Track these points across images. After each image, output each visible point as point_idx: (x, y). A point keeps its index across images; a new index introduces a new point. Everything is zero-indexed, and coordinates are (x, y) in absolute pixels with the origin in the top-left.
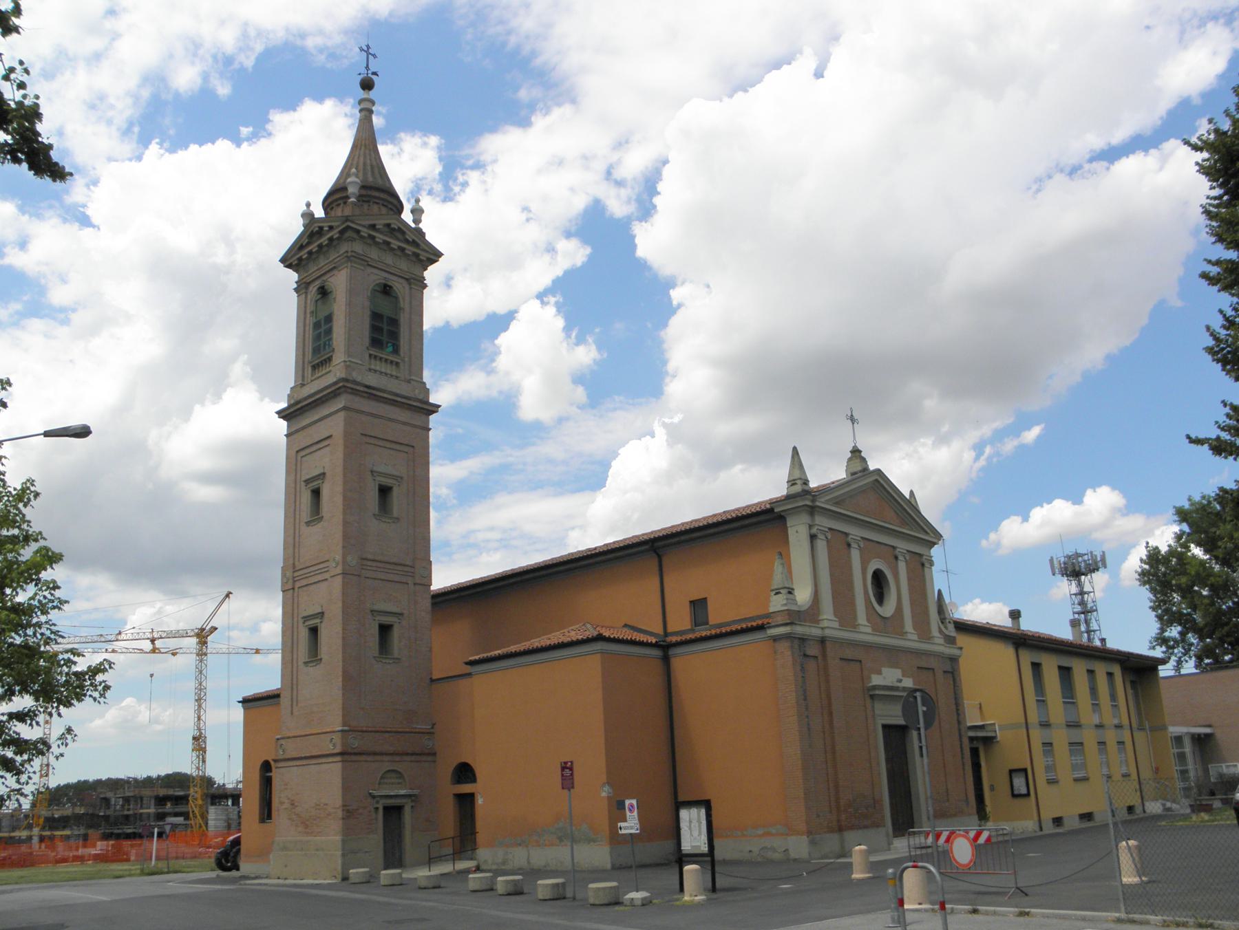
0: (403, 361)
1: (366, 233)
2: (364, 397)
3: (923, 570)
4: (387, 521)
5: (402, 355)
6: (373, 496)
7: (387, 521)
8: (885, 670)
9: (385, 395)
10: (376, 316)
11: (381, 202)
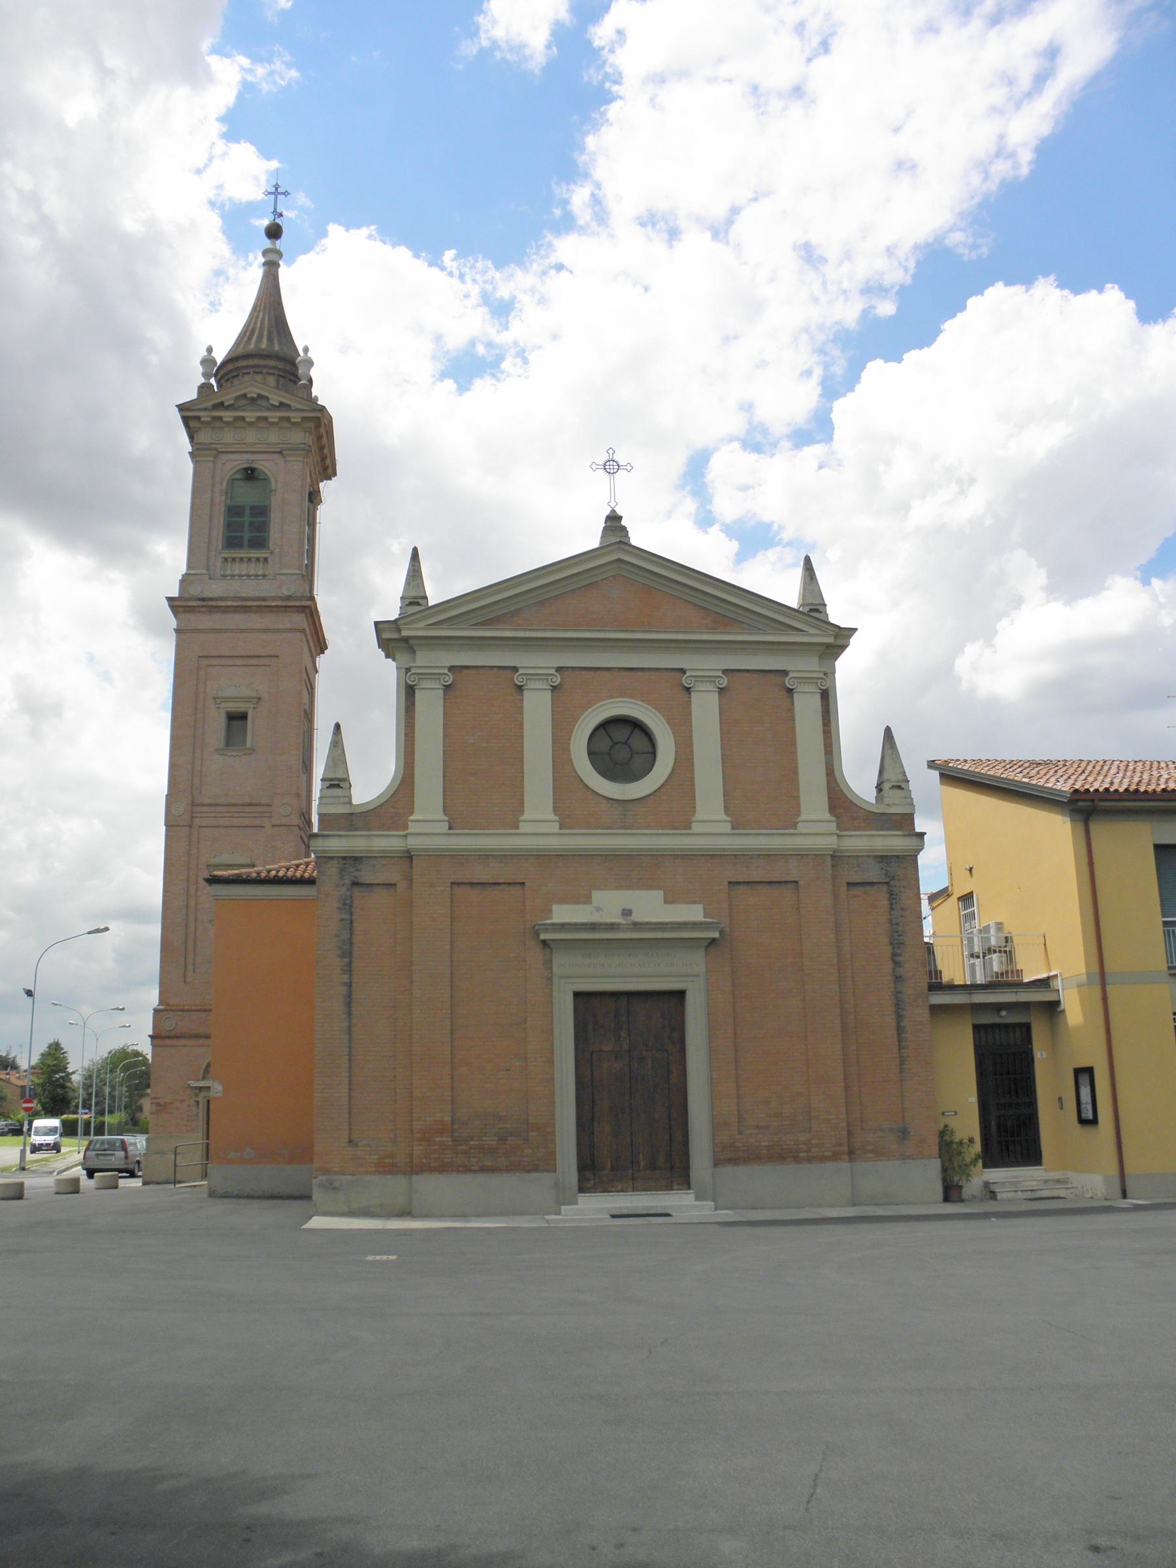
0: (272, 553)
1: (208, 416)
2: (203, 612)
3: (792, 698)
4: (234, 754)
5: (271, 546)
6: (216, 724)
7: (234, 754)
8: (597, 895)
9: (229, 603)
10: (234, 511)
11: (251, 370)
